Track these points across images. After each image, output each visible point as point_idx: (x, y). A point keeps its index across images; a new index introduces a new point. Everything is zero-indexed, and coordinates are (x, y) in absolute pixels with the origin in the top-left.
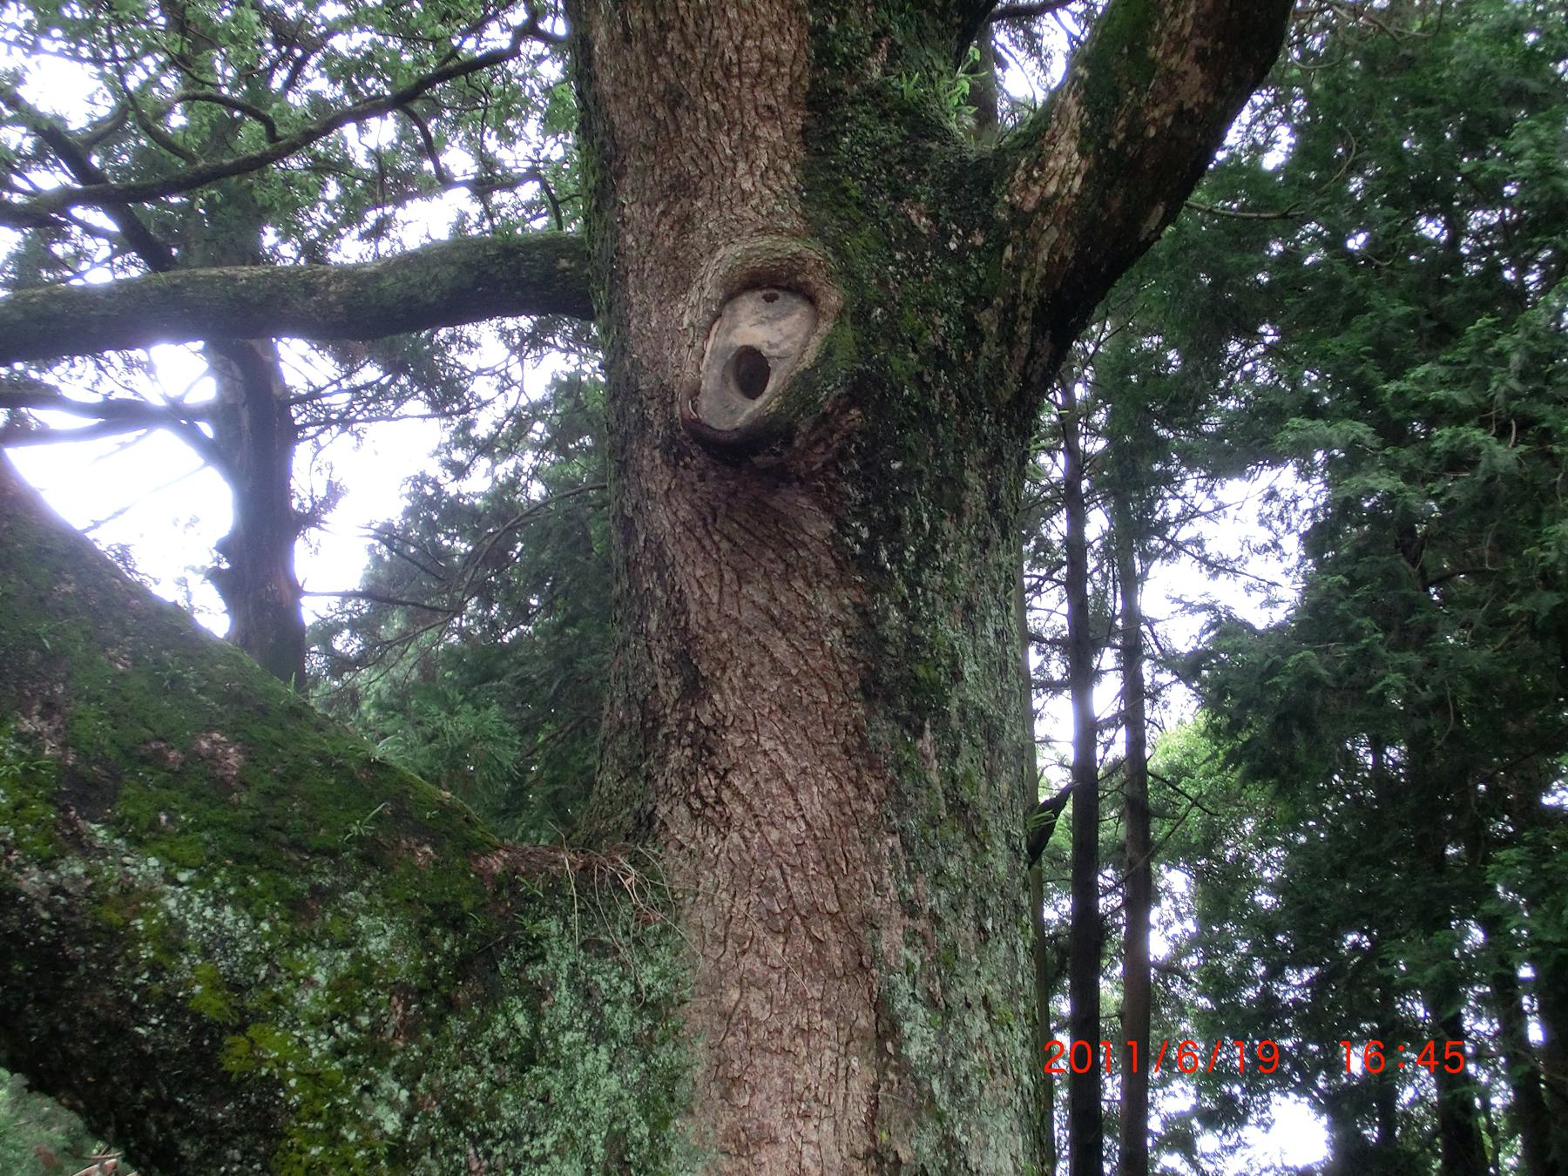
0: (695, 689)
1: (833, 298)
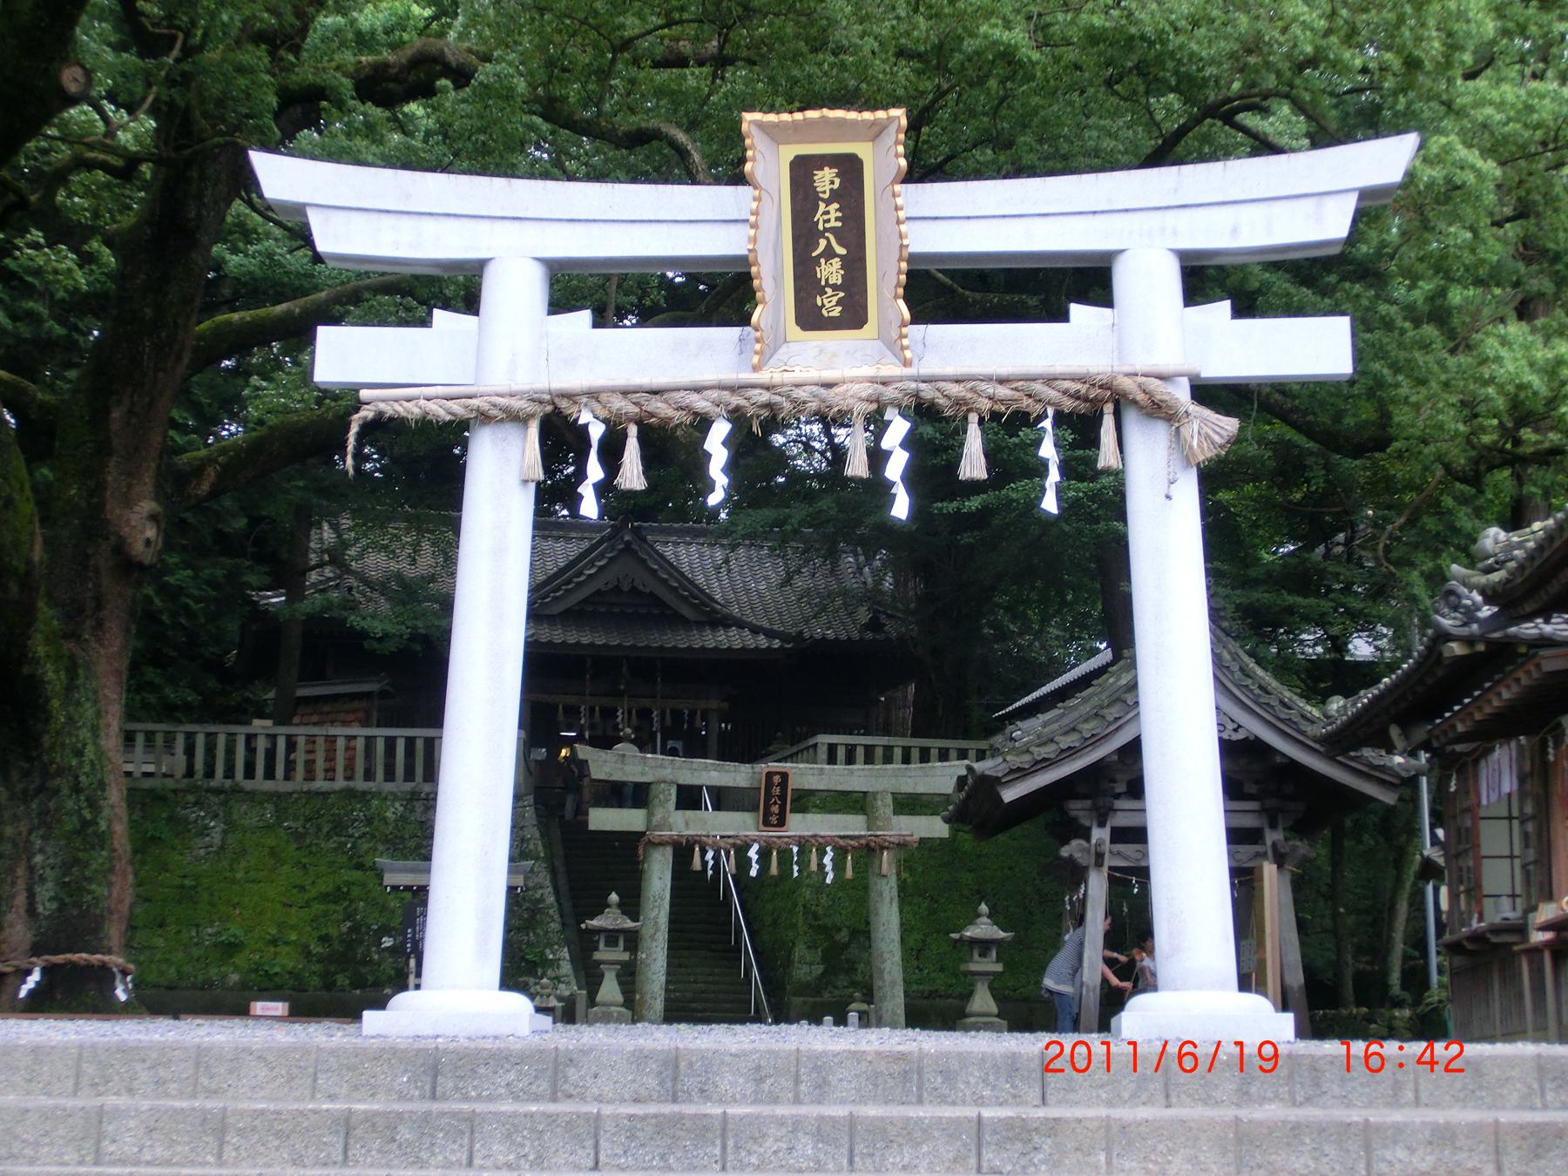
0: (99, 607)
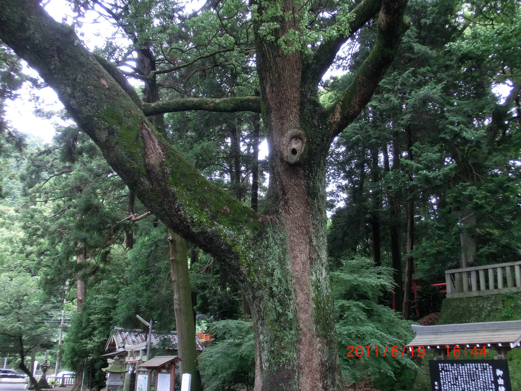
0: (284, 194)
1: (305, 140)
